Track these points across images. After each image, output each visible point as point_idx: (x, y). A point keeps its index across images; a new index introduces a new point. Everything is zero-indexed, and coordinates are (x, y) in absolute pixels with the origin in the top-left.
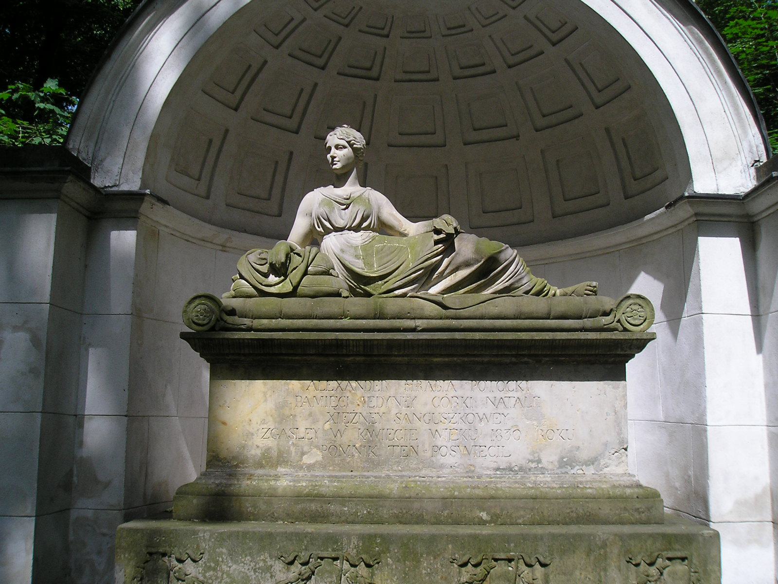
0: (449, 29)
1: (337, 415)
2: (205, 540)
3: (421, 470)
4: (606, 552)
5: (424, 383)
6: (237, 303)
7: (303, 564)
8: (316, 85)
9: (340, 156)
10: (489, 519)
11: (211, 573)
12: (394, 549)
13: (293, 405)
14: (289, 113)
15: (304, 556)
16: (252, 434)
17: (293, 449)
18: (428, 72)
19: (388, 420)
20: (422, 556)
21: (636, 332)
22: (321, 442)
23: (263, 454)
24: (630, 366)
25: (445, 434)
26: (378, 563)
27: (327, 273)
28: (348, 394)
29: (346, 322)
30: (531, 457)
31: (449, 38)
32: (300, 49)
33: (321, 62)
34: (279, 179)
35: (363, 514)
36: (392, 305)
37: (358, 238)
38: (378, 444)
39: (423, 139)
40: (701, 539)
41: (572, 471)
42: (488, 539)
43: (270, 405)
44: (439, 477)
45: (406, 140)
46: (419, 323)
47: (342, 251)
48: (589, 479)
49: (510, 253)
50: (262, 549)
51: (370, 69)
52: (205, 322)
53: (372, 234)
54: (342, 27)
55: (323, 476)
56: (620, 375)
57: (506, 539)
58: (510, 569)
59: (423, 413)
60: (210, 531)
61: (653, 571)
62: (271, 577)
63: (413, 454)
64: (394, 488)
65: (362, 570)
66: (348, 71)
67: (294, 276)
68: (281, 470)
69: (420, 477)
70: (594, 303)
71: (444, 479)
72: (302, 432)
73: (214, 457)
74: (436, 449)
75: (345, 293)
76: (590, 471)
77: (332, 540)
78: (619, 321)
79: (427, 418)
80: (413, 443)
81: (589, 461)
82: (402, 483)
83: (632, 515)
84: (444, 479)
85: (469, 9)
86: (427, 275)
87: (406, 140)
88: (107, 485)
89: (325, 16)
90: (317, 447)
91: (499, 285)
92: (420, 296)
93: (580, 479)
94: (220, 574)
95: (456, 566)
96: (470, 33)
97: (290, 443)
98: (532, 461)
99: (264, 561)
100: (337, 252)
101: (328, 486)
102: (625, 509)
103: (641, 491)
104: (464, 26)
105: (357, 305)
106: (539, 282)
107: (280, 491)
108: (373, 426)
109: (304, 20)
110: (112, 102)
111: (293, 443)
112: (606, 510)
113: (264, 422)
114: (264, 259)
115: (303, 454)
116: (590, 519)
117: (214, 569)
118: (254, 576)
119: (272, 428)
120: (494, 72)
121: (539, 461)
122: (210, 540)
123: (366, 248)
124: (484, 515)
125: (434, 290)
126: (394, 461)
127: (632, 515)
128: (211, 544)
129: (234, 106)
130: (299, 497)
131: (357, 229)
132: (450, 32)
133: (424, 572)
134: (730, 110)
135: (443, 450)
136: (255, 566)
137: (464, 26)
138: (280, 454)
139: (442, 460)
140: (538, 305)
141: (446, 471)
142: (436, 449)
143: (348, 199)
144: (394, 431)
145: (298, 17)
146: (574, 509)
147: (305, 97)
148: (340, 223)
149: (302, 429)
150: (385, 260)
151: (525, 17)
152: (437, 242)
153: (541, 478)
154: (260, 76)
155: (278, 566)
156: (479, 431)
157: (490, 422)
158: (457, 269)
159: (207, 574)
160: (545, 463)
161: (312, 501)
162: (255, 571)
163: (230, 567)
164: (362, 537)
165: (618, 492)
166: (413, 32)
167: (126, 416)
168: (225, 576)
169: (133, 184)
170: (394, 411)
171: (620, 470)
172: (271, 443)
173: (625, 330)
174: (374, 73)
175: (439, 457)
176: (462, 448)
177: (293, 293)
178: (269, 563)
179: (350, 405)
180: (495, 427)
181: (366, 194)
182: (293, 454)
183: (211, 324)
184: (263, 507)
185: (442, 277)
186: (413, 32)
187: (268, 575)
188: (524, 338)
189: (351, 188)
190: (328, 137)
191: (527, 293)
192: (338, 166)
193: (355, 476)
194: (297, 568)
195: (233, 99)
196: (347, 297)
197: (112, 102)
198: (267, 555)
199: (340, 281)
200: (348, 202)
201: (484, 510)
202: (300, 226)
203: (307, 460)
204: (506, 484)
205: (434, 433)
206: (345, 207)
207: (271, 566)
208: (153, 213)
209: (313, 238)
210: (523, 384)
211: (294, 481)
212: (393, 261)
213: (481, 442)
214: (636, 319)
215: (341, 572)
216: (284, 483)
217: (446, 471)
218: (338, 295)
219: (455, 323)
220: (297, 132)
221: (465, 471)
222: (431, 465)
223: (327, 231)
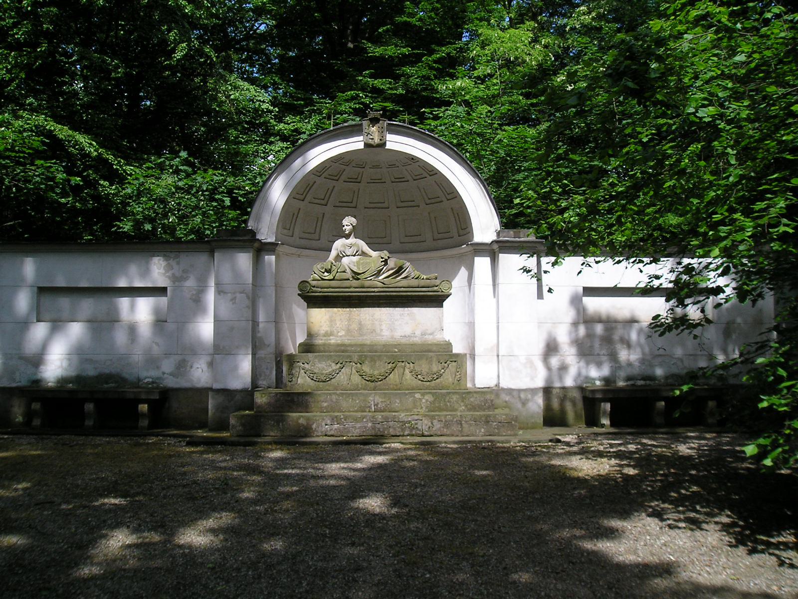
1: (349, 320)
5: (377, 309)
6: (314, 283)
8: (334, 187)
9: (347, 229)
12: (368, 359)
15: (341, 362)
21: (446, 292)
24: (444, 303)
27: (344, 272)
29: (352, 290)
34: (319, 224)
36: (367, 283)
39: (380, 205)
42: (396, 356)
43: (327, 317)
45: (372, 205)
49: (408, 264)
53: (359, 257)
56: (442, 306)
57: (402, 356)
61: (446, 365)
64: (368, 342)
65: (359, 365)
66: (348, 180)
67: (334, 273)
68: (331, 337)
70: (434, 282)
72: (338, 325)
74: (381, 330)
76: (431, 337)
77: (350, 357)
86: (379, 273)
87: (372, 205)
91: (403, 276)
101: (347, 342)
105: (355, 283)
106: (417, 273)
112: (434, 349)
116: (430, 351)
123: (357, 262)
125: (381, 278)
130: (338, 345)
131: (354, 256)
134: (489, 211)
138: (331, 332)
139: (383, 334)
140: (415, 283)
147: (329, 191)
155: (333, 364)
160: (416, 334)
169: (272, 239)
172: (328, 329)
174: (358, 180)
177: (333, 279)
184: (327, 349)
185: (383, 273)
189: (352, 240)
192: (347, 232)
194: (339, 365)
199: (349, 275)
202: (333, 253)
203: (340, 334)
204: (404, 341)
205: (381, 325)
208: (280, 249)
209: (338, 258)
210: (409, 309)
215: (352, 366)
216: (333, 341)
219: (387, 289)
223: (344, 256)
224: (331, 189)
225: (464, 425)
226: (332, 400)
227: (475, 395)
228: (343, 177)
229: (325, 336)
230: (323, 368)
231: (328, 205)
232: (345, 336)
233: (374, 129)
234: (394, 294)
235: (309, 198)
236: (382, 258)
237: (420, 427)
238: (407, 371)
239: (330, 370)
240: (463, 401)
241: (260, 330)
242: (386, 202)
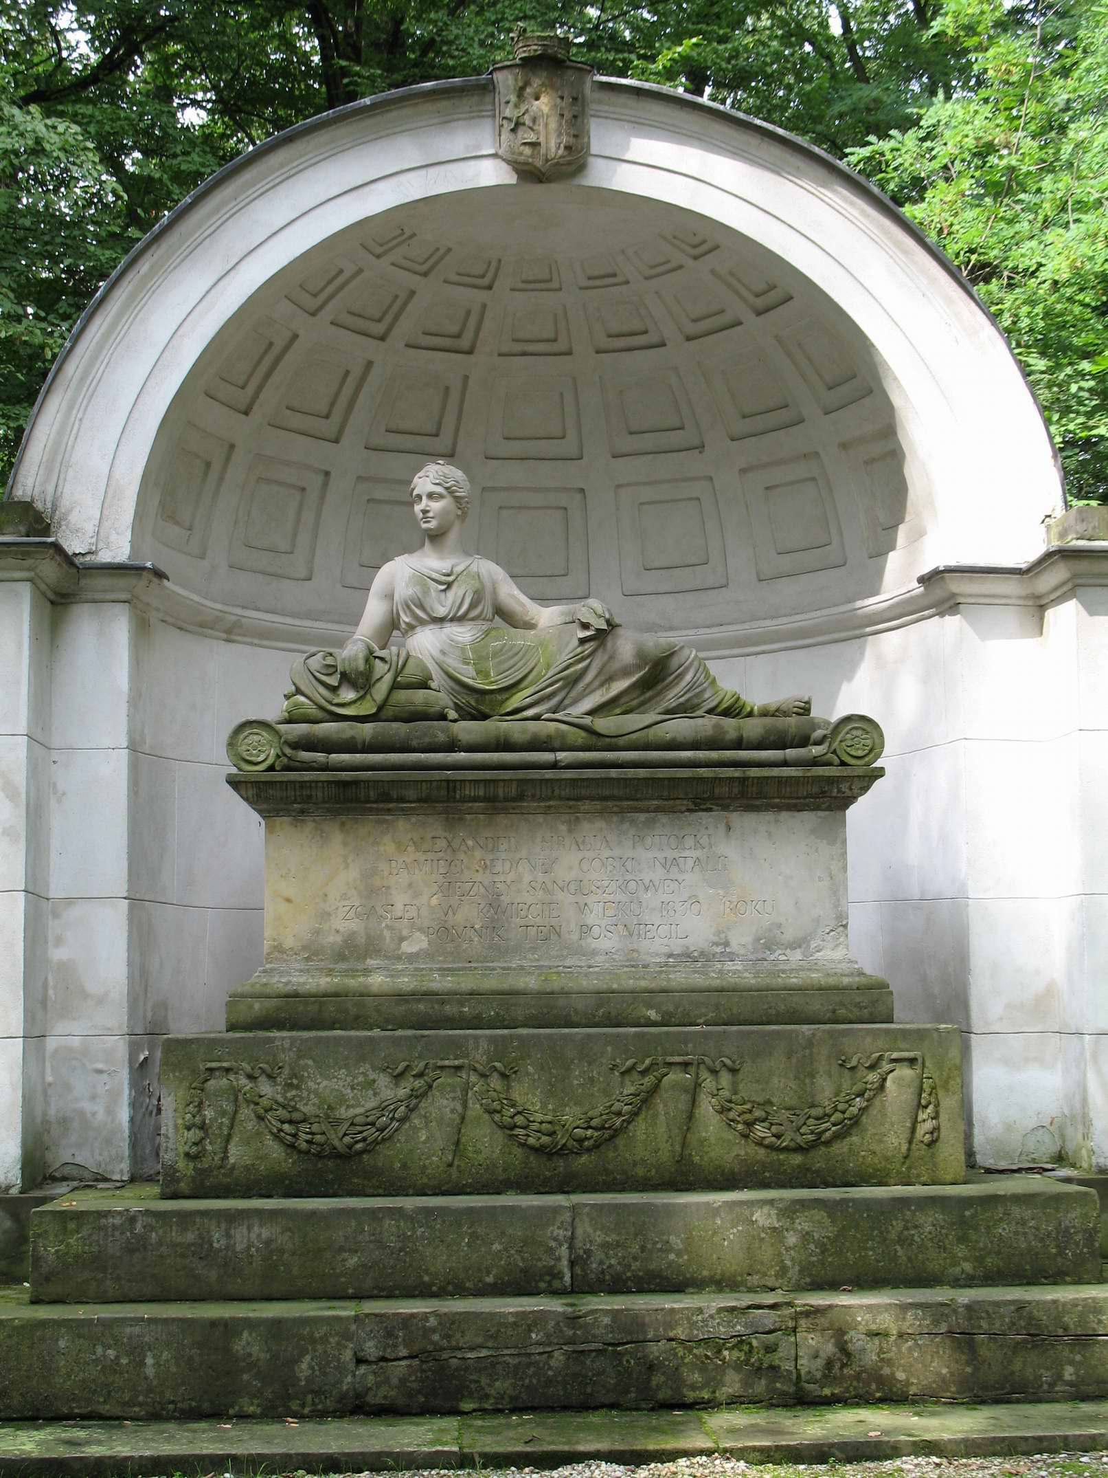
0: (590, 278)
2: (283, 1050)
3: (565, 958)
4: (811, 1054)
7: (416, 1076)
8: (370, 364)
10: (659, 1019)
11: (294, 1092)
13: (386, 873)
14: (325, 411)
16: (329, 914)
17: (387, 934)
18: (555, 340)
19: (519, 891)
20: (572, 1062)
22: (426, 924)
23: (345, 941)
25: (598, 909)
26: (515, 1072)
28: (462, 856)
30: (716, 939)
31: (589, 292)
32: (348, 312)
33: (379, 328)
35: (490, 1016)
37: (464, 634)
38: (506, 925)
40: (935, 1035)
41: (772, 957)
44: (590, 967)
45: (516, 448)
46: (561, 755)
47: (443, 653)
48: (794, 967)
50: (362, 1059)
51: (458, 336)
52: (260, 759)
54: (417, 278)
55: (431, 969)
58: (688, 1076)
59: (567, 880)
60: (290, 1038)
61: (873, 1077)
62: (375, 1094)
63: (554, 937)
64: (531, 982)
65: (495, 1082)
67: (380, 691)
68: (371, 962)
69: (565, 967)
71: (597, 969)
72: (398, 910)
73: (275, 947)
75: (452, 714)
76: (797, 955)
78: (834, 752)
79: (572, 888)
80: (554, 922)
81: (794, 942)
82: (540, 975)
83: (851, 1011)
84: (597, 969)
85: (623, 252)
88: (101, 1001)
89: (393, 264)
90: (420, 930)
92: (560, 718)
93: (781, 967)
94: (305, 1094)
95: (617, 1074)
96: (624, 287)
97: (383, 925)
98: (717, 944)
99: (365, 1074)
100: (436, 654)
101: (438, 983)
102: (842, 1004)
103: (863, 980)
104: (614, 275)
107: (375, 989)
108: (498, 899)
109: (360, 271)
110: (77, 422)
111: (387, 925)
112: (816, 1006)
113: (344, 897)
114: (333, 666)
115: (402, 939)
117: (298, 1087)
118: (352, 1095)
119: (357, 904)
120: (663, 344)
121: (727, 944)
122: (290, 1049)
124: (652, 1014)
126: (528, 946)
127: (851, 1011)
128: (291, 1054)
129: (243, 408)
130: (401, 997)
132: (591, 283)
133: (576, 1082)
135: (596, 930)
136: (353, 1081)
137: (614, 275)
139: (595, 944)
141: (600, 959)
142: (585, 929)
143: (449, 575)
144: (527, 906)
145: (349, 269)
146: (773, 1004)
148: (441, 611)
149: (399, 907)
150: (506, 666)
151: (713, 272)
152: (583, 641)
153: (729, 966)
154: (287, 357)
155: (383, 1080)
156: (644, 904)
157: (660, 891)
158: (611, 679)
159: (289, 1095)
160: (735, 946)
161: (419, 1001)
162: (353, 1088)
163: (319, 1084)
164: (492, 1040)
165: (832, 981)
166: (530, 282)
167: (125, 898)
168: (312, 1096)
169: (118, 549)
170: (527, 878)
171: (838, 954)
172: (355, 925)
173: (843, 764)
175: (590, 940)
176: (621, 927)
178: (371, 1077)
179: (465, 871)
180: (666, 898)
181: (474, 568)
182: (388, 940)
183: (269, 762)
186: (530, 282)
187: (371, 1092)
188: (704, 775)
190: (416, 479)
191: (710, 711)
193: (475, 968)
195: (244, 397)
196: (455, 721)
197: (77, 422)
198: (367, 1066)
200: (451, 579)
201: (652, 1008)
202: (374, 611)
203: (407, 948)
204: (680, 977)
205: (582, 908)
206: (443, 587)
207: (374, 1081)
211: (392, 976)
212: (516, 667)
213: (647, 918)
214: (858, 749)
216: (377, 981)
217: (600, 959)
218: (443, 717)
220: (337, 441)
221: (625, 959)
222: (580, 952)
223: (422, 623)
224: (356, 371)
225: (983, 1352)
226: (380, 1244)
227: (1016, 1211)
228: (406, 327)
229: (341, 957)
230: (342, 1099)
231: (345, 441)
232: (428, 955)
233: (543, 105)
234: (642, 773)
235: (270, 398)
236: (585, 626)
237: (787, 1366)
238: (707, 1107)
239: (371, 1104)
240: (962, 1239)
241: (1096, 1132)
242: (572, 434)
